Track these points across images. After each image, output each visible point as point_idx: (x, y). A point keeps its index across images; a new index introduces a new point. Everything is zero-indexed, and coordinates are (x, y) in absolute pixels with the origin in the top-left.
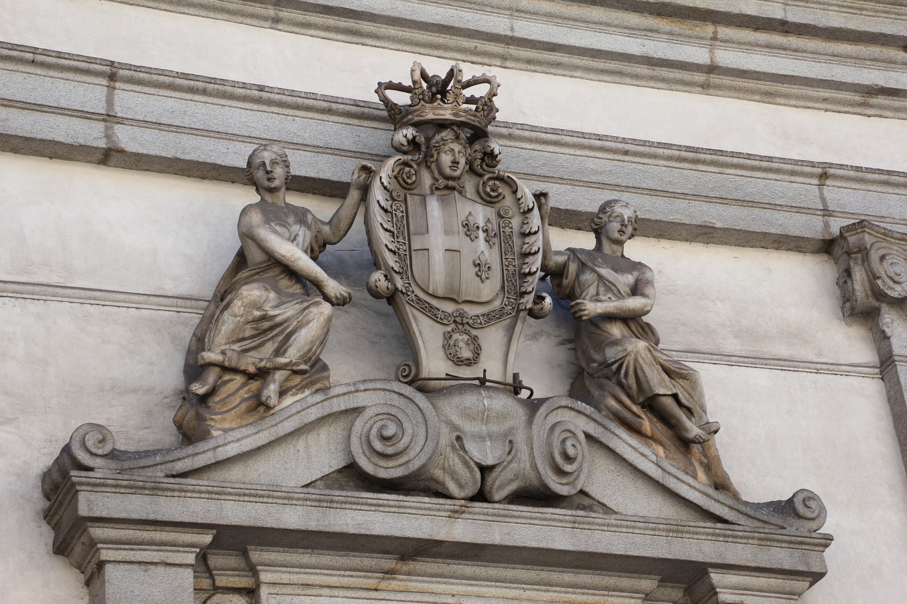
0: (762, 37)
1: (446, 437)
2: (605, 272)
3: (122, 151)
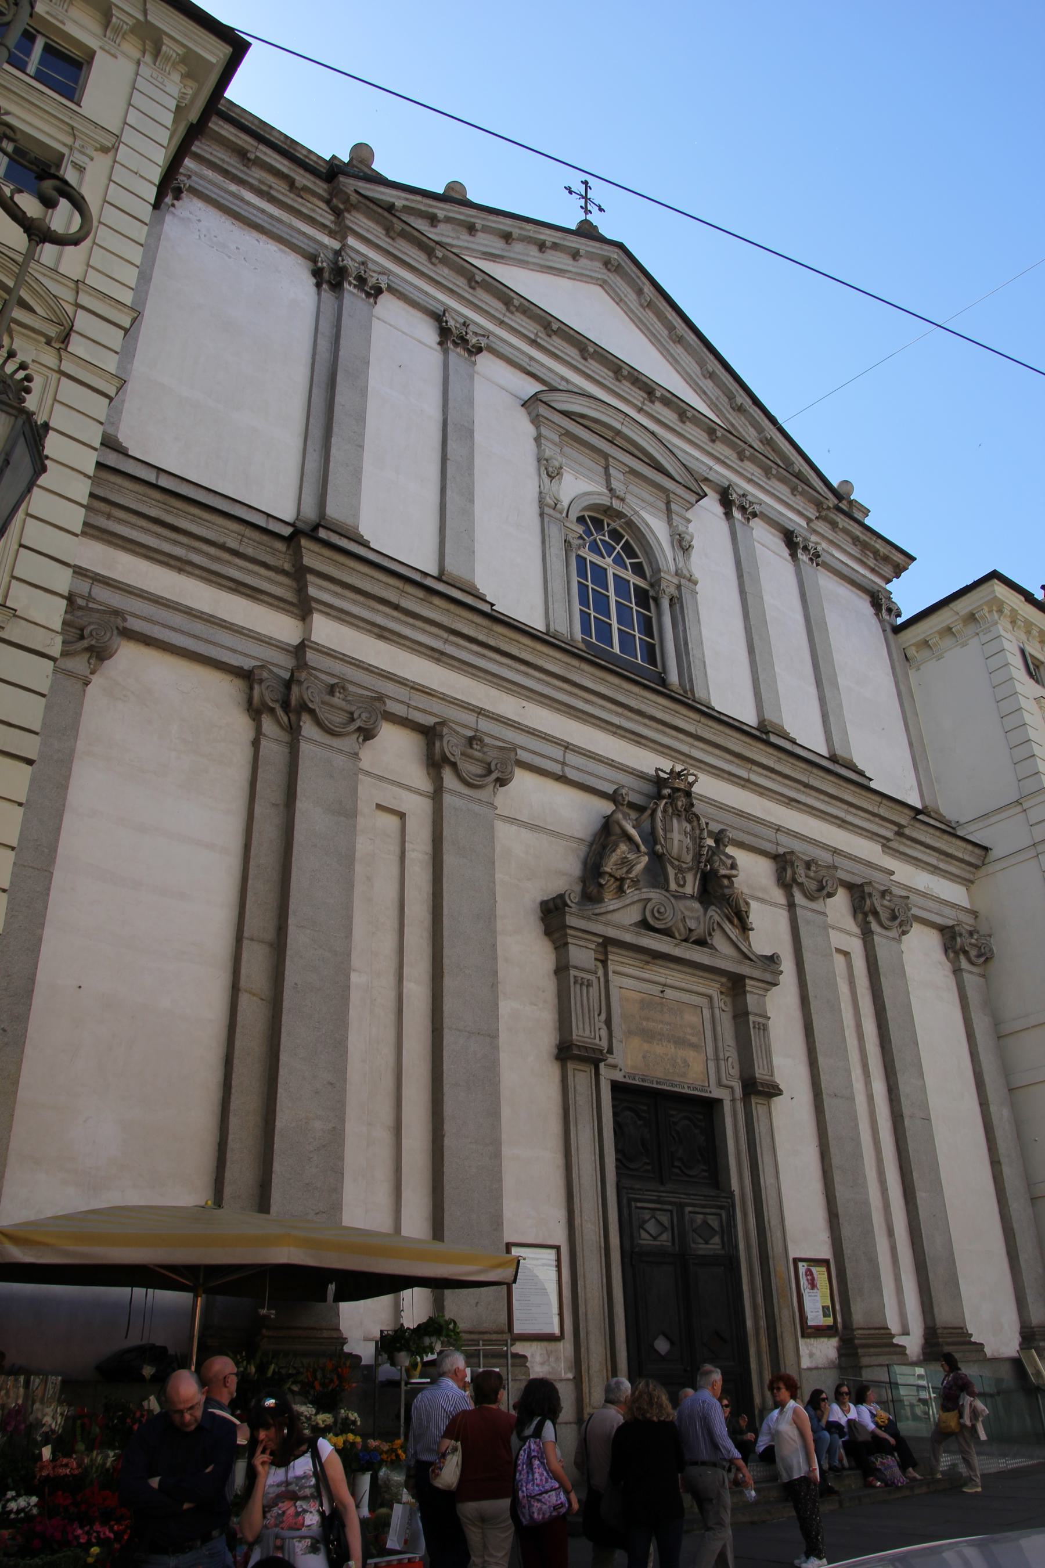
0: (765, 772)
1: (680, 917)
2: (723, 857)
3: (566, 777)
